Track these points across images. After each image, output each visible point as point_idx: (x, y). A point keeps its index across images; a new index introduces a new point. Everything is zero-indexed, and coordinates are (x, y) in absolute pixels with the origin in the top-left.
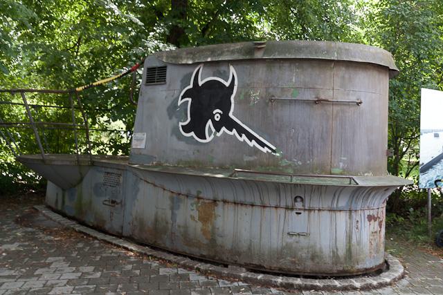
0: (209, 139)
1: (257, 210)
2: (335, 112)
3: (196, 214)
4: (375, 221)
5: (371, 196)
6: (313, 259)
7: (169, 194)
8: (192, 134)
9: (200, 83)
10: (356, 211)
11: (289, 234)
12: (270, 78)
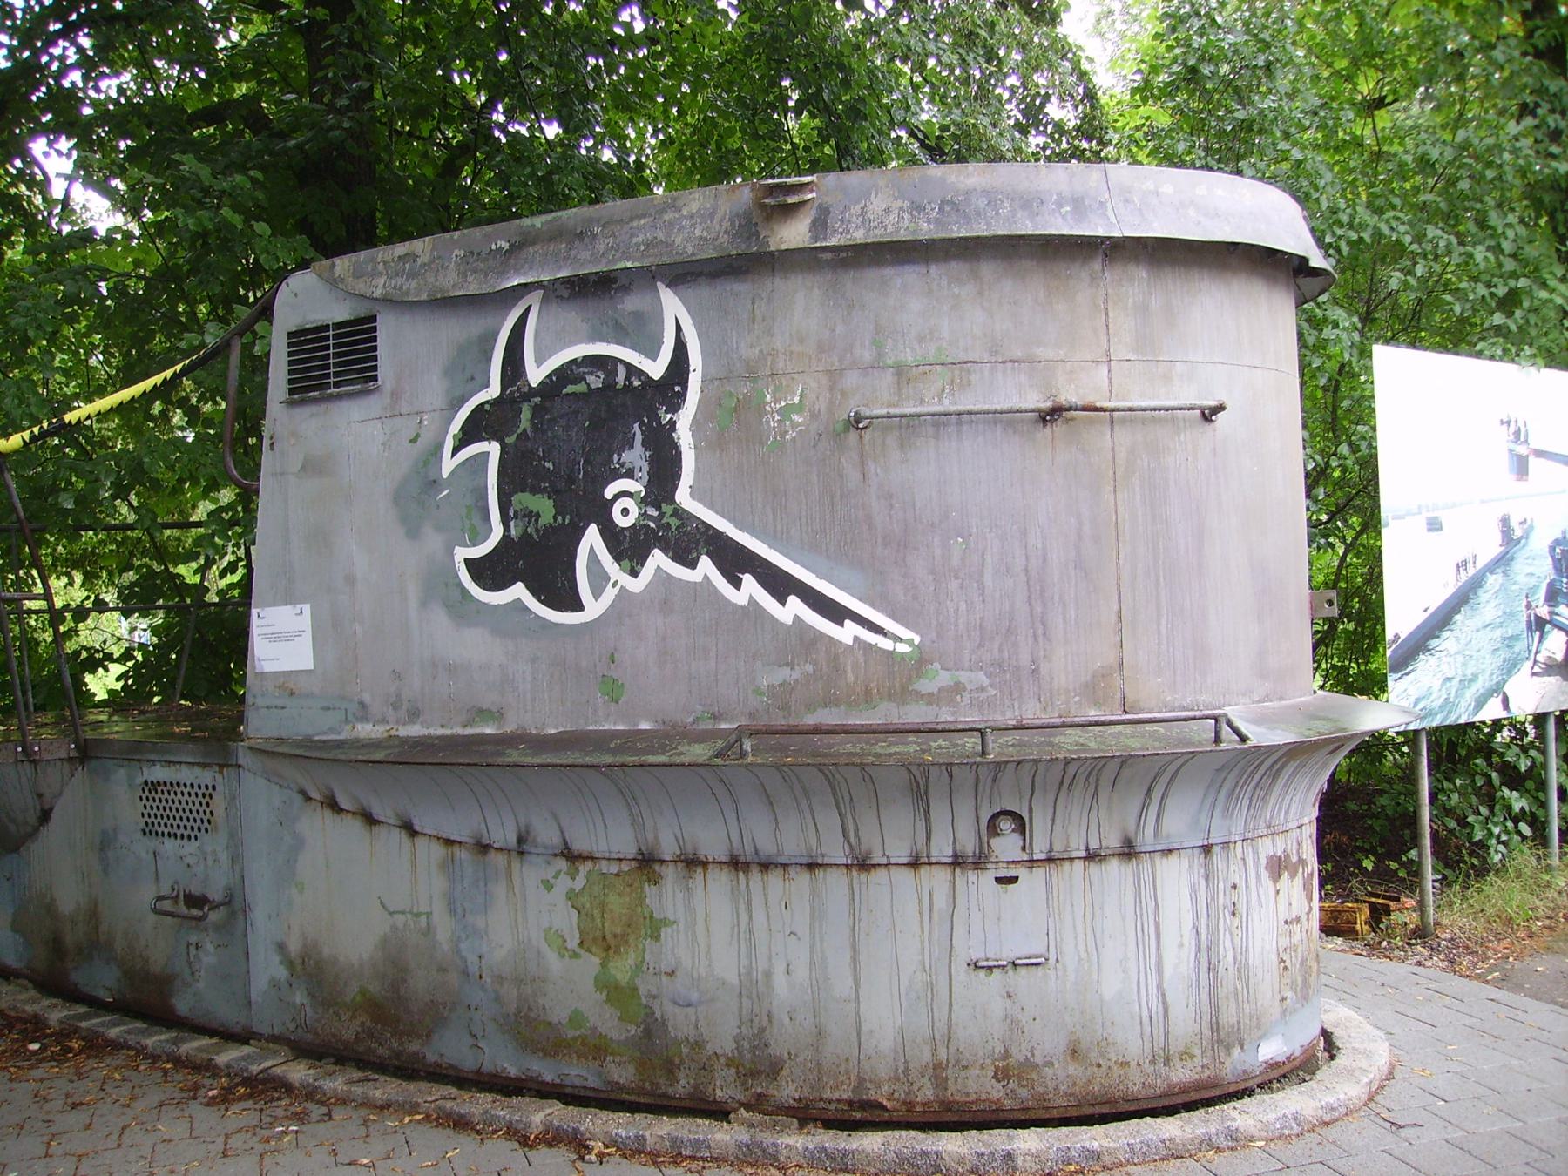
0: (594, 608)
1: (835, 883)
2: (1122, 455)
3: (566, 920)
4: (1293, 875)
5: (1281, 781)
6: (1074, 1052)
7: (438, 851)
8: (519, 591)
9: (535, 374)
10: (1226, 845)
11: (976, 966)
12: (840, 329)
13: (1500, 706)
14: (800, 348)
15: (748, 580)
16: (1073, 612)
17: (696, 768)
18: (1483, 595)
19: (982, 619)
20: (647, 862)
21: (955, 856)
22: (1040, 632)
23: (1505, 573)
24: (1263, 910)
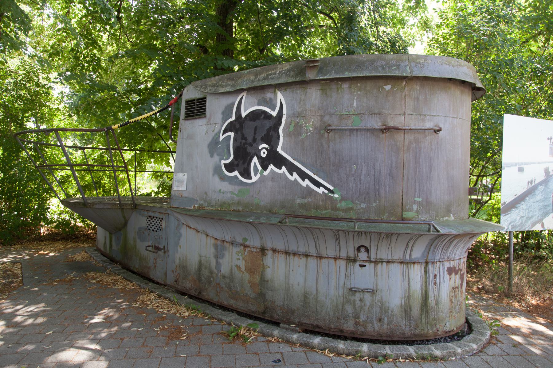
0: (255, 179)
1: (312, 262)
2: (407, 143)
4: (456, 274)
7: (213, 241)
8: (236, 173)
9: (244, 114)
10: (433, 263)
12: (325, 103)
13: (541, 226)
14: (313, 109)
16: (388, 189)
18: (537, 192)
19: (360, 189)
20: (263, 250)
21: (347, 257)
22: (377, 194)
23: (545, 186)
24: (445, 284)
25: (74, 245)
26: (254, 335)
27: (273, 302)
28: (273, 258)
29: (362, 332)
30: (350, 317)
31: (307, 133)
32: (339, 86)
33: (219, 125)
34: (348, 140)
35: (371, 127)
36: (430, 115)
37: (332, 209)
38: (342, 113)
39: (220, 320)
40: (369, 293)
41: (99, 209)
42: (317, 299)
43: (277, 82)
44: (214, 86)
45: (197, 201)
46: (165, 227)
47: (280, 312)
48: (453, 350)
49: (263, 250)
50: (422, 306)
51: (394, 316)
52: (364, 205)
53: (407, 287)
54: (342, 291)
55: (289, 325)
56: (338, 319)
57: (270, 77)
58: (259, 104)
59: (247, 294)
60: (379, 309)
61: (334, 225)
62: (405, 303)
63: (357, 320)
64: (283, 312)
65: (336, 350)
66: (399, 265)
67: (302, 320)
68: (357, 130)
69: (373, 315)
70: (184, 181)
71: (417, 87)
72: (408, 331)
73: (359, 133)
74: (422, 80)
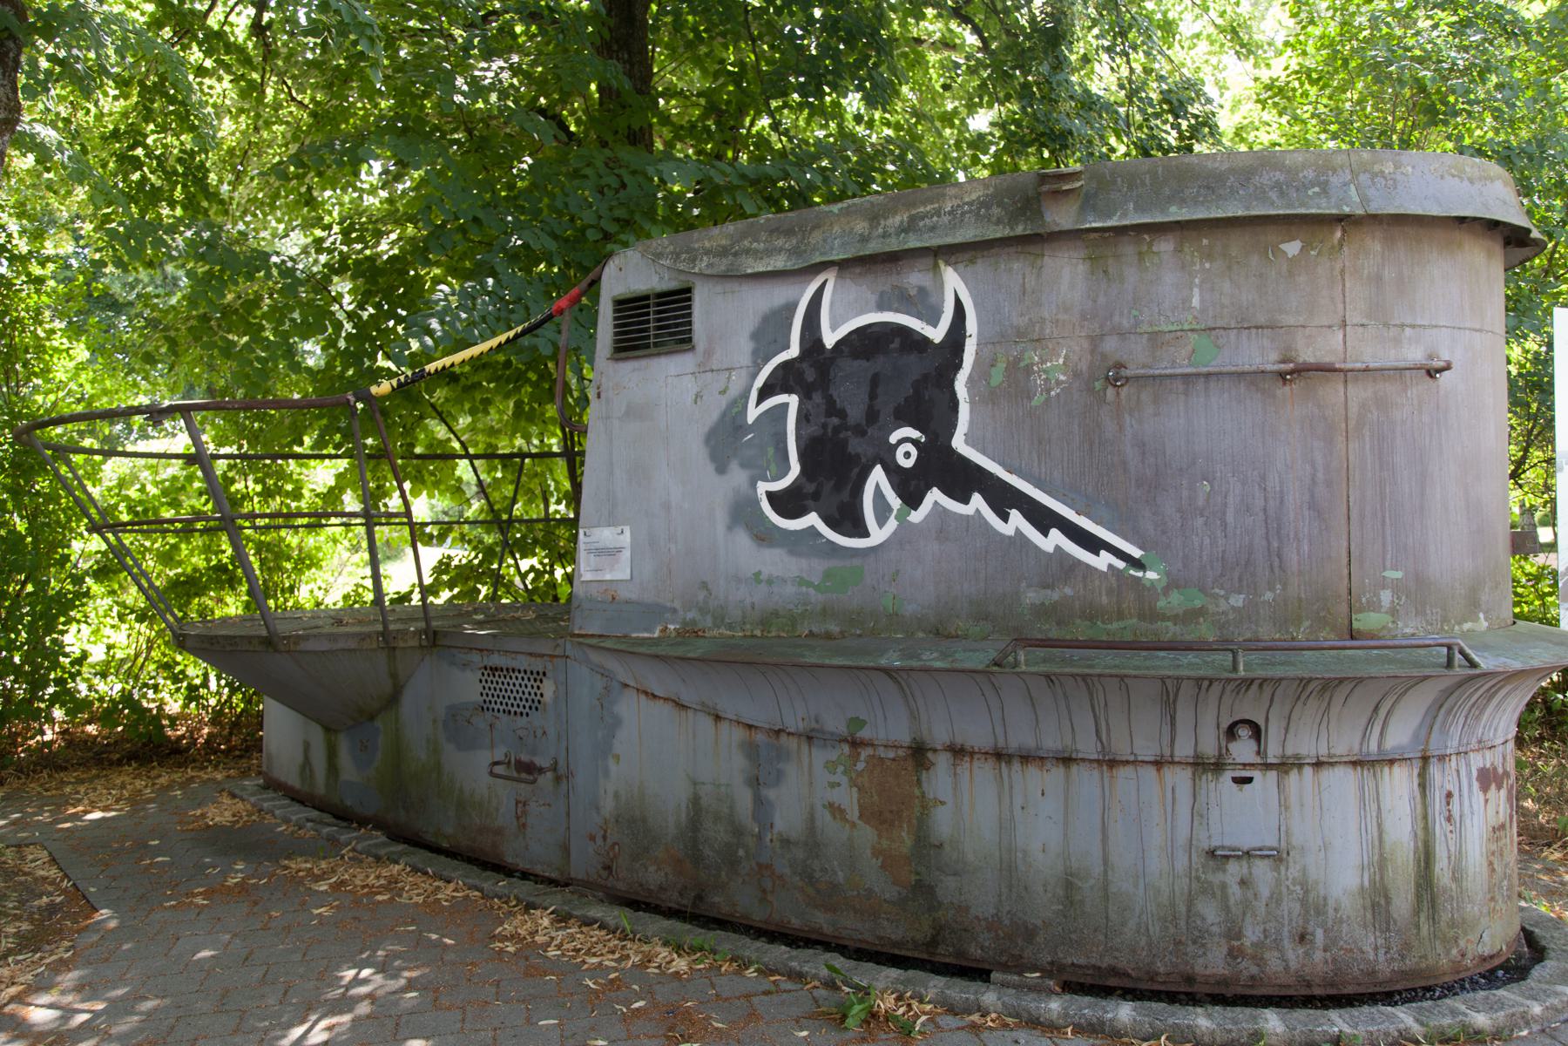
0: (878, 535)
1: (1087, 780)
2: (1354, 409)
4: (1499, 787)
7: (739, 734)
8: (812, 519)
9: (830, 339)
10: (1442, 758)
12: (1102, 300)
14: (1066, 317)
15: (1015, 515)
16: (1306, 548)
17: (974, 675)
19: (1224, 552)
20: (919, 753)
21: (1196, 756)
22: (1276, 563)
24: (1475, 817)
25: (176, 776)
26: (924, 1013)
27: (963, 909)
28: (955, 774)
29: (1252, 977)
30: (1211, 935)
31: (1048, 391)
32: (1145, 248)
33: (744, 373)
34: (1181, 408)
35: (1254, 368)
36: (1413, 326)
37: (1142, 617)
38: (1156, 329)
39: (797, 977)
40: (1266, 861)
41: (315, 652)
42: (1105, 887)
43: (949, 240)
44: (723, 252)
45: (674, 611)
46: (556, 699)
47: (986, 939)
48: (1522, 1009)
49: (919, 753)
50: (1418, 886)
51: (1341, 921)
52: (1238, 601)
53: (1376, 834)
54: (1186, 859)
55: (1020, 974)
56: (1178, 943)
57: (921, 224)
58: (881, 307)
59: (870, 891)
60: (1298, 905)
61: (1164, 663)
62: (1372, 882)
63: (1236, 943)
64: (997, 935)
65: (1190, 1037)
66: (1349, 770)
67: (1061, 955)
68: (1208, 375)
69: (1283, 925)
70: (619, 550)
71: (1374, 244)
72: (1385, 967)
73: (1212, 384)
74: (1388, 224)
